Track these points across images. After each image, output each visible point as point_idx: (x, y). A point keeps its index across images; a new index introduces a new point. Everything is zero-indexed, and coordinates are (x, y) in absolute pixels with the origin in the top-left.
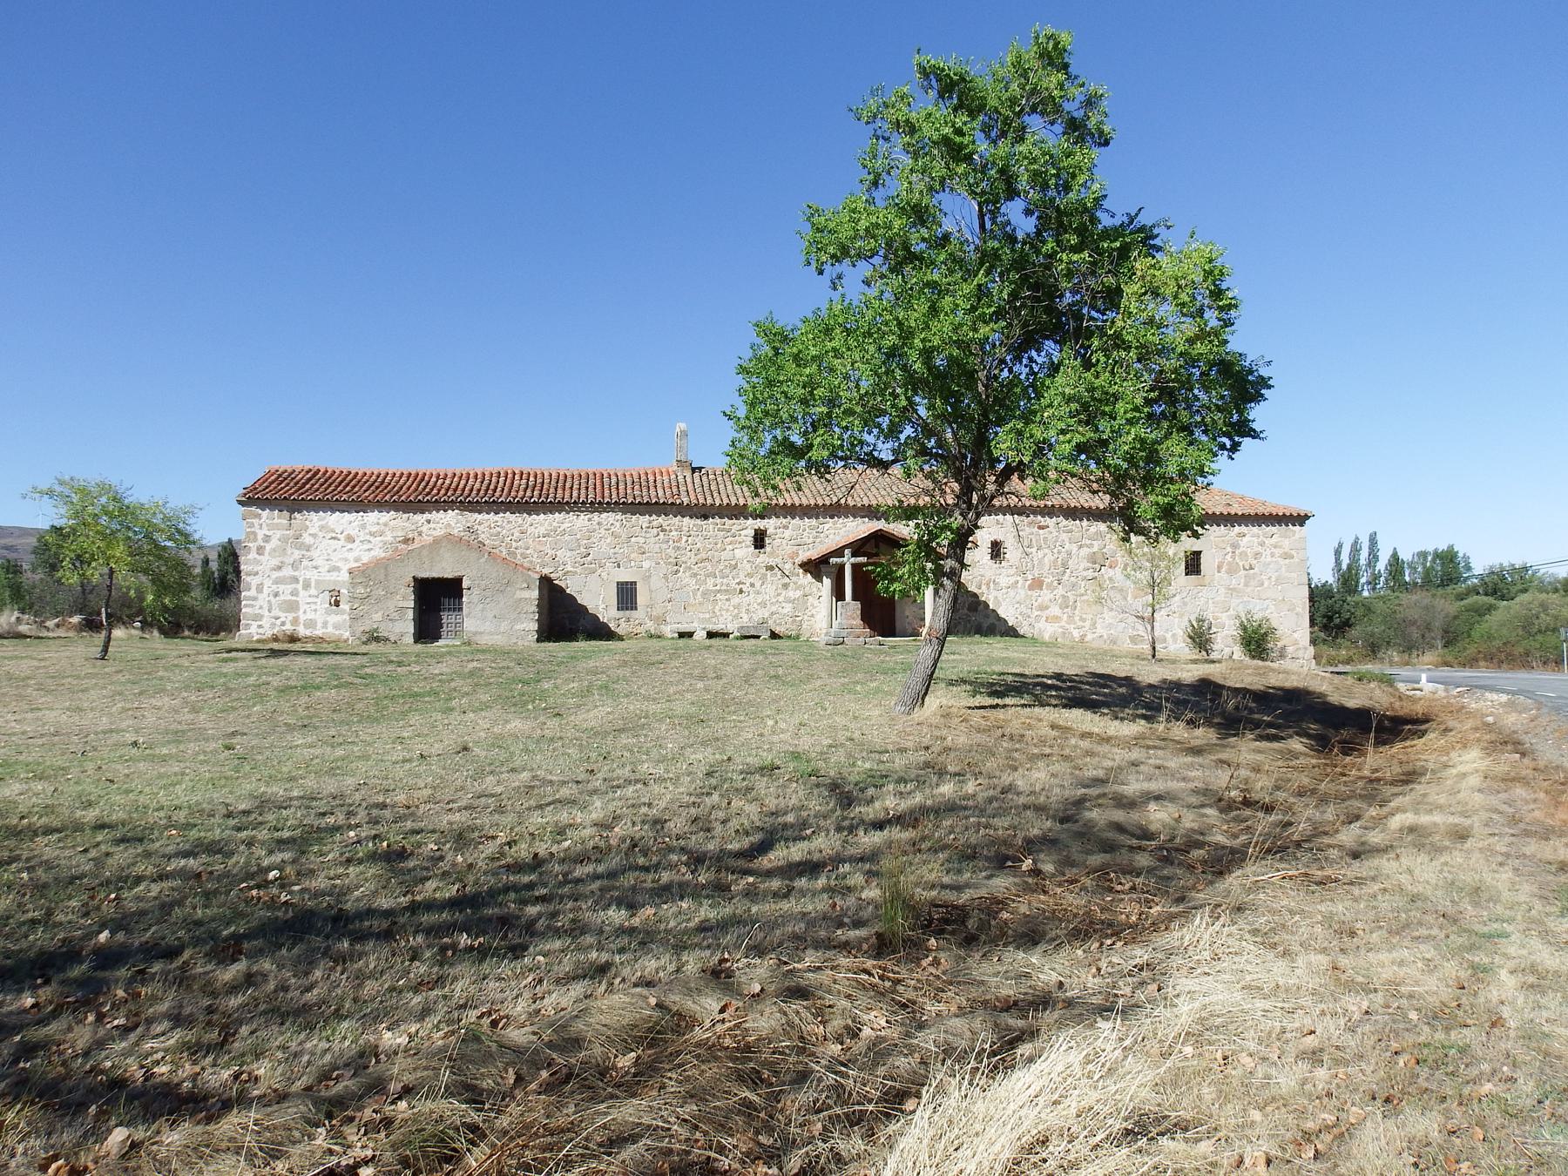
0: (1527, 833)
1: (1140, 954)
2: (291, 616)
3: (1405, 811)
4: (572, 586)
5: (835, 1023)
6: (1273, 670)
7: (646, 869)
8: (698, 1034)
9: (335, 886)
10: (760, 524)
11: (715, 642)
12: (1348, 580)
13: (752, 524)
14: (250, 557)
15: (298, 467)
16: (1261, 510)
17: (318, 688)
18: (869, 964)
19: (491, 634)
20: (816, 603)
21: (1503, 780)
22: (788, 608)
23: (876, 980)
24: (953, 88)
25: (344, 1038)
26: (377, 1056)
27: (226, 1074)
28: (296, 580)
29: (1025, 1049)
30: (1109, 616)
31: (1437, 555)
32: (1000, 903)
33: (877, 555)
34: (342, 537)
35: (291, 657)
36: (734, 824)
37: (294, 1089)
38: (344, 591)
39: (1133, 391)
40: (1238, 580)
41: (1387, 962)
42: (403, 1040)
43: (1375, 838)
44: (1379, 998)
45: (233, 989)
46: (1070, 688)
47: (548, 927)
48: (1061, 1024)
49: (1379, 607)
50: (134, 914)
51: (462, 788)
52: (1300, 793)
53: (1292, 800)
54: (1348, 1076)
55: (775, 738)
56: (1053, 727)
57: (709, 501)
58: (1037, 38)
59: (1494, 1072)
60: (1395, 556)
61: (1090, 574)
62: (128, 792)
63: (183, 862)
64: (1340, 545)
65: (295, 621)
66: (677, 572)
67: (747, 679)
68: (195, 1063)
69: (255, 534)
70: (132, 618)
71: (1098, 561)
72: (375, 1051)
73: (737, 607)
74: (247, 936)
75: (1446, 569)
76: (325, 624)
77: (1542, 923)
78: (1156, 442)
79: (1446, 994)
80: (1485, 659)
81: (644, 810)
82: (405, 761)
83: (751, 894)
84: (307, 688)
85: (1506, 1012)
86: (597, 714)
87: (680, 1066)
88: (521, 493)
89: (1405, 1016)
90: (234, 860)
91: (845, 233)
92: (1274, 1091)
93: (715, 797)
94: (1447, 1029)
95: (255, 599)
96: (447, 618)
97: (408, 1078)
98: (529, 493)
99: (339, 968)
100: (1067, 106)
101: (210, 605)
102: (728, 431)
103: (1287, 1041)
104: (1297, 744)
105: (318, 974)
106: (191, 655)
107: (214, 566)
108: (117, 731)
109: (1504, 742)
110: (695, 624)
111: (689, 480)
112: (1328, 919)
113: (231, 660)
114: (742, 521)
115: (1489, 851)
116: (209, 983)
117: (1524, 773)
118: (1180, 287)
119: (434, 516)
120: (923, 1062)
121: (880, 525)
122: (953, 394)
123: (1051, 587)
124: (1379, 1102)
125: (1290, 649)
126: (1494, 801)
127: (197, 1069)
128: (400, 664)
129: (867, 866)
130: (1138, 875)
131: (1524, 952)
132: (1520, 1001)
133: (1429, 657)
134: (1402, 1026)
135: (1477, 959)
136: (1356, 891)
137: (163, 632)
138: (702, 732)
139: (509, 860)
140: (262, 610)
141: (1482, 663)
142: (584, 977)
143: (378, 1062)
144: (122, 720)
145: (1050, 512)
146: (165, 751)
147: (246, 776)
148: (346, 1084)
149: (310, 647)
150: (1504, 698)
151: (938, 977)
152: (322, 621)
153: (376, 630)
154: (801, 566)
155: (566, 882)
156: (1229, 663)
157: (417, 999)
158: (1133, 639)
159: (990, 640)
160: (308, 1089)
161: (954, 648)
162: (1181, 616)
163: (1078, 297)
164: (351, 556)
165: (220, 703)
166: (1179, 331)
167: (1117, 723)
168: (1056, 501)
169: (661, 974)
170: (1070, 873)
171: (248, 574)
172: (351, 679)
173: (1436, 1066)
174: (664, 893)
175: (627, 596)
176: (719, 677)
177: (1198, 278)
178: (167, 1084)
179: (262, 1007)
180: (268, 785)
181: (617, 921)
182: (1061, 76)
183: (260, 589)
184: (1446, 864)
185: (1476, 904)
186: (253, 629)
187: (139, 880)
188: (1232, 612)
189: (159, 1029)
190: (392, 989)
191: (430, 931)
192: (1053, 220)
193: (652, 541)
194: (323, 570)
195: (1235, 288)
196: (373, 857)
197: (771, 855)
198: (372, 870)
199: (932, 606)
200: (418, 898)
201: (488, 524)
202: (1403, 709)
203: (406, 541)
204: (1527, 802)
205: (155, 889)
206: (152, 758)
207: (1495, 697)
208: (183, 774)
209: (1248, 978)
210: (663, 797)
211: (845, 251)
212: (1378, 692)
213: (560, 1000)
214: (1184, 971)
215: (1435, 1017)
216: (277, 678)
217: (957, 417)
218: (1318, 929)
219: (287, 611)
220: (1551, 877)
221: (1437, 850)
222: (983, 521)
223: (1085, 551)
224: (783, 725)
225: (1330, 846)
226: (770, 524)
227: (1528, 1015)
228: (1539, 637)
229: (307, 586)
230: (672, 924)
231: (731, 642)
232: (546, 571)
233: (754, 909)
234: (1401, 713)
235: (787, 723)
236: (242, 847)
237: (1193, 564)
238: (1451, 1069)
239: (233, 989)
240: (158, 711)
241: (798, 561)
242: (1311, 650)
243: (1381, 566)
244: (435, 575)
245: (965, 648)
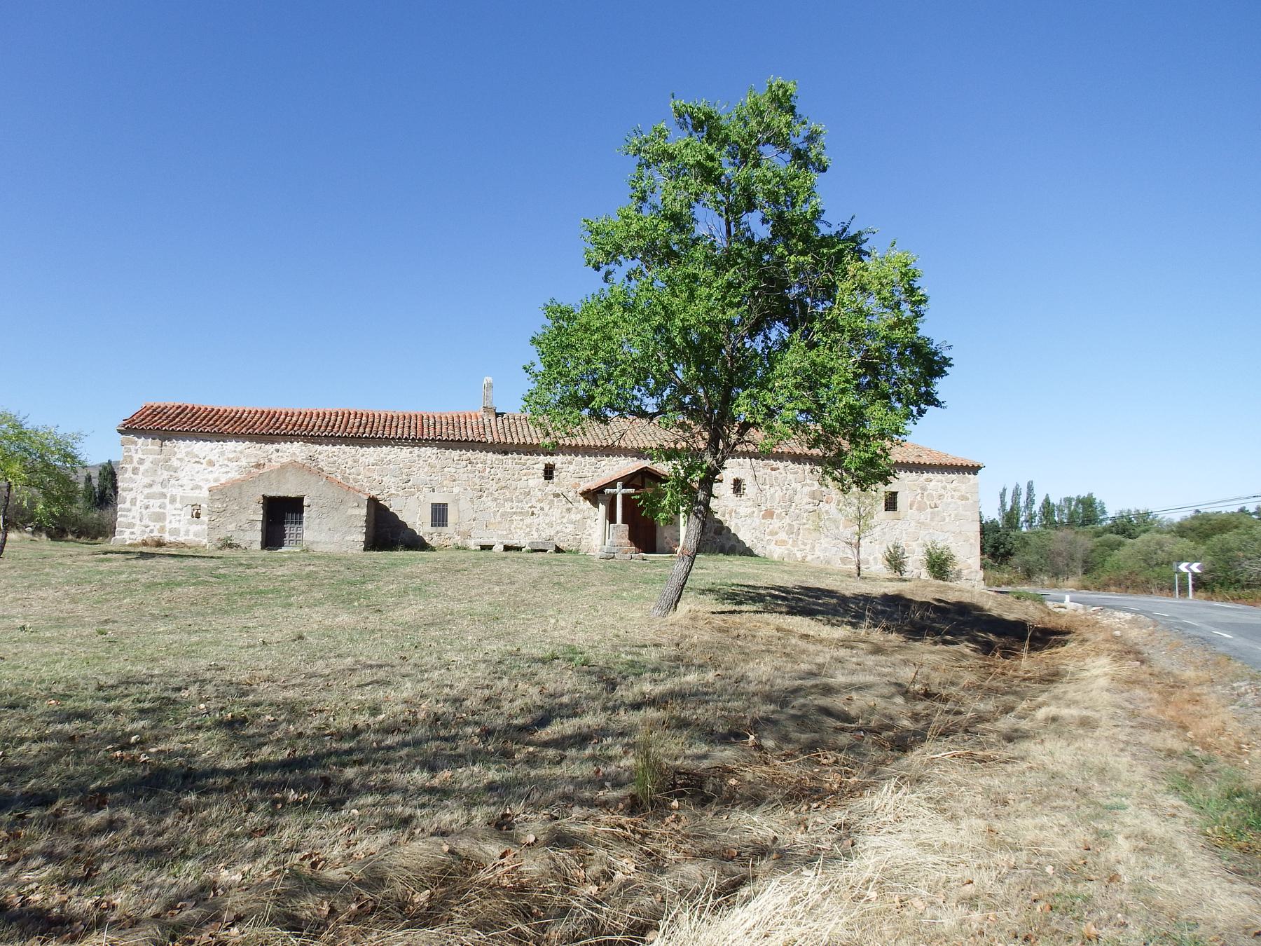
0: (1143, 726)
1: (840, 816)
2: (158, 525)
3: (1048, 705)
4: (394, 506)
5: (594, 868)
6: (952, 589)
7: (446, 739)
8: (482, 875)
9: (186, 749)
10: (550, 460)
11: (510, 554)
12: (1011, 518)
13: (543, 460)
14: (126, 476)
15: (170, 403)
16: (944, 461)
17: (179, 585)
18: (624, 820)
19: (326, 543)
20: (593, 524)
21: (1126, 682)
22: (570, 528)
23: (629, 833)
24: (705, 125)
25: (188, 874)
26: (215, 890)
27: (88, 903)
28: (164, 495)
29: (745, 891)
30: (825, 542)
31: (1079, 501)
32: (726, 771)
33: (643, 487)
34: (204, 461)
35: (157, 559)
36: (519, 703)
37: (144, 916)
38: (204, 506)
39: (846, 364)
40: (925, 516)
41: (1030, 826)
42: (238, 877)
43: (1024, 725)
44: (1023, 856)
45: (97, 831)
46: (794, 598)
47: (363, 785)
48: (772, 873)
49: (1034, 540)
50: (17, 768)
51: (297, 670)
52: (967, 689)
53: (962, 693)
54: (996, 917)
55: (556, 634)
56: (778, 630)
57: (509, 440)
58: (771, 86)
59: (1110, 918)
60: (1047, 501)
61: (811, 507)
62: (15, 668)
63: (59, 727)
64: (1004, 490)
65: (162, 529)
66: (481, 496)
67: (535, 584)
68: (63, 893)
69: (131, 457)
70: (24, 524)
71: (817, 498)
72: (213, 886)
73: (529, 526)
74: (112, 789)
75: (1087, 511)
76: (187, 533)
77: (1152, 798)
78: (861, 407)
79: (1075, 854)
80: (1115, 585)
81: (447, 690)
82: (249, 646)
83: (531, 761)
84: (170, 585)
85: (1121, 870)
86: (412, 610)
87: (465, 902)
88: (355, 430)
89: (1043, 871)
90: (102, 726)
91: (618, 236)
92: (938, 929)
93: (505, 681)
94: (1075, 882)
95: (129, 510)
96: (289, 529)
97: (241, 909)
98: (361, 430)
99: (187, 817)
100: (793, 140)
101: (90, 515)
102: (528, 384)
103: (951, 890)
104: (965, 648)
105: (169, 821)
106: (73, 556)
107: (95, 482)
108: (9, 617)
109: (1128, 652)
110: (495, 539)
111: (493, 423)
112: (987, 790)
113: (109, 560)
114: (535, 457)
115: (1113, 739)
116: (77, 827)
117: (1142, 677)
118: (881, 284)
119: (282, 446)
120: (663, 901)
121: (646, 463)
122: (705, 362)
123: (780, 517)
124: (1019, 940)
125: (965, 572)
126: (1118, 698)
127: (65, 898)
128: (249, 566)
129: (626, 740)
130: (841, 751)
131: (1137, 822)
132: (1133, 861)
133: (1072, 581)
134: (1040, 878)
135: (1100, 826)
136: (1009, 768)
137: (52, 537)
138: (497, 627)
139: (333, 730)
140: (134, 520)
141: (1113, 588)
142: (391, 827)
143: (216, 895)
144: (13, 608)
145: (780, 457)
146: (48, 634)
147: (116, 657)
148: (190, 912)
149: (173, 551)
150: (1129, 616)
151: (678, 832)
152: (182, 529)
153: (229, 538)
154: (582, 494)
155: (379, 748)
156: (918, 583)
157: (251, 844)
158: (844, 561)
159: (731, 558)
160: (157, 916)
161: (702, 564)
162: (881, 543)
163: (803, 290)
164: (211, 477)
165: (97, 596)
166: (881, 320)
167: (828, 628)
168: (785, 449)
169: (454, 826)
170: (787, 748)
171: (124, 490)
172: (208, 578)
173: (1066, 911)
174: (458, 760)
175: (439, 515)
176: (512, 583)
177: (896, 278)
178: (40, 909)
179: (121, 848)
180: (133, 664)
181: (420, 782)
182: (789, 118)
183: (133, 502)
184: (1080, 748)
185: (1102, 782)
186: (126, 535)
187: (22, 741)
188: (920, 541)
189: (34, 864)
190: (230, 835)
191: (262, 786)
192: (783, 227)
193: (462, 472)
194: (188, 488)
195: (924, 286)
196: (220, 724)
197: (549, 730)
198: (220, 734)
199: (686, 531)
200: (255, 760)
201: (325, 453)
202: (1051, 623)
203: (258, 466)
204: (1144, 701)
205: (36, 748)
206: (36, 641)
207: (1121, 615)
208: (63, 654)
209: (923, 837)
210: (461, 681)
211: (619, 248)
212: (1031, 608)
213: (369, 845)
214: (873, 830)
215: (1066, 873)
216: (145, 576)
217: (707, 380)
218: (979, 798)
219: (155, 521)
220: (1160, 762)
221: (1073, 738)
222: (728, 463)
223: (807, 489)
224: (562, 623)
225: (990, 731)
226: (558, 460)
227: (1138, 873)
228: (1157, 569)
229: (173, 500)
230: (465, 784)
231: (523, 554)
232: (373, 493)
233: (533, 773)
234: (1049, 626)
235: (566, 621)
236: (110, 716)
237: (891, 503)
238: (1076, 914)
239: (97, 831)
240: (44, 601)
241: (580, 490)
242: (981, 573)
243: (1036, 508)
244: (281, 494)
245: (711, 564)
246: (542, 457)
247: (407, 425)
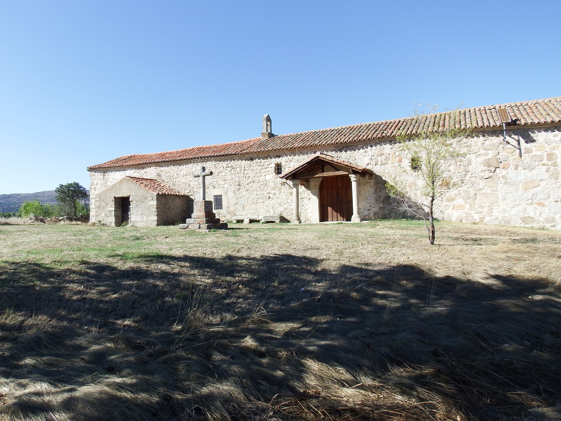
10: (278, 160)
13: (274, 161)
20: (308, 202)
61: (487, 174)
114: (269, 160)
246: (273, 160)
247: (407, 127)
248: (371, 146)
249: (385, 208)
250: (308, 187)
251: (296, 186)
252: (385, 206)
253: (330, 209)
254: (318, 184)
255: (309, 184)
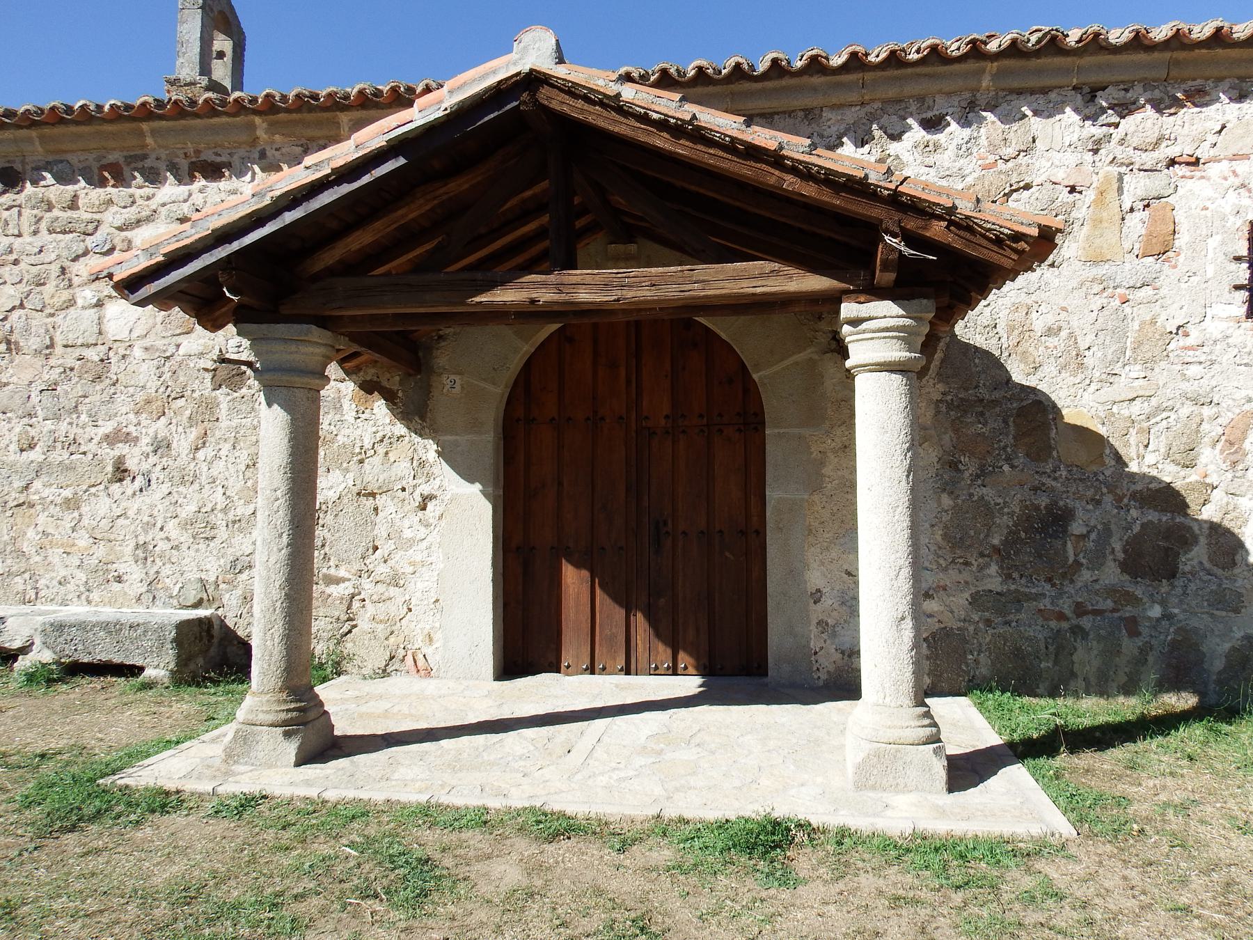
20: (410, 526)
114: (139, 189)
246: (170, 190)
248: (933, 124)
249: (1018, 600)
250: (416, 411)
251: (295, 392)
252: (1020, 585)
253: (574, 580)
254: (498, 391)
255: (426, 391)
